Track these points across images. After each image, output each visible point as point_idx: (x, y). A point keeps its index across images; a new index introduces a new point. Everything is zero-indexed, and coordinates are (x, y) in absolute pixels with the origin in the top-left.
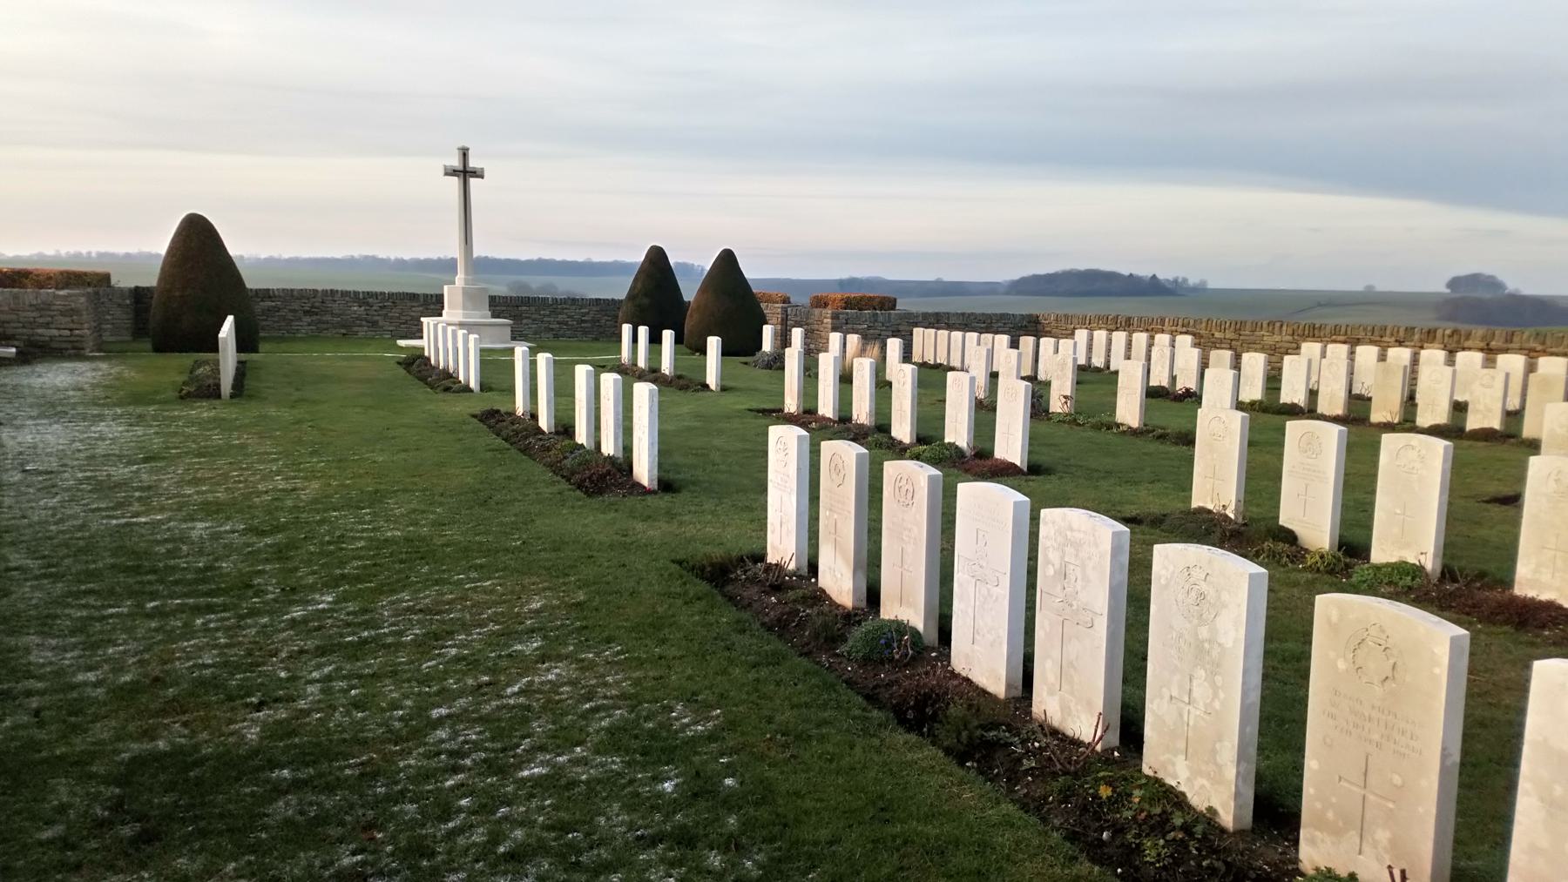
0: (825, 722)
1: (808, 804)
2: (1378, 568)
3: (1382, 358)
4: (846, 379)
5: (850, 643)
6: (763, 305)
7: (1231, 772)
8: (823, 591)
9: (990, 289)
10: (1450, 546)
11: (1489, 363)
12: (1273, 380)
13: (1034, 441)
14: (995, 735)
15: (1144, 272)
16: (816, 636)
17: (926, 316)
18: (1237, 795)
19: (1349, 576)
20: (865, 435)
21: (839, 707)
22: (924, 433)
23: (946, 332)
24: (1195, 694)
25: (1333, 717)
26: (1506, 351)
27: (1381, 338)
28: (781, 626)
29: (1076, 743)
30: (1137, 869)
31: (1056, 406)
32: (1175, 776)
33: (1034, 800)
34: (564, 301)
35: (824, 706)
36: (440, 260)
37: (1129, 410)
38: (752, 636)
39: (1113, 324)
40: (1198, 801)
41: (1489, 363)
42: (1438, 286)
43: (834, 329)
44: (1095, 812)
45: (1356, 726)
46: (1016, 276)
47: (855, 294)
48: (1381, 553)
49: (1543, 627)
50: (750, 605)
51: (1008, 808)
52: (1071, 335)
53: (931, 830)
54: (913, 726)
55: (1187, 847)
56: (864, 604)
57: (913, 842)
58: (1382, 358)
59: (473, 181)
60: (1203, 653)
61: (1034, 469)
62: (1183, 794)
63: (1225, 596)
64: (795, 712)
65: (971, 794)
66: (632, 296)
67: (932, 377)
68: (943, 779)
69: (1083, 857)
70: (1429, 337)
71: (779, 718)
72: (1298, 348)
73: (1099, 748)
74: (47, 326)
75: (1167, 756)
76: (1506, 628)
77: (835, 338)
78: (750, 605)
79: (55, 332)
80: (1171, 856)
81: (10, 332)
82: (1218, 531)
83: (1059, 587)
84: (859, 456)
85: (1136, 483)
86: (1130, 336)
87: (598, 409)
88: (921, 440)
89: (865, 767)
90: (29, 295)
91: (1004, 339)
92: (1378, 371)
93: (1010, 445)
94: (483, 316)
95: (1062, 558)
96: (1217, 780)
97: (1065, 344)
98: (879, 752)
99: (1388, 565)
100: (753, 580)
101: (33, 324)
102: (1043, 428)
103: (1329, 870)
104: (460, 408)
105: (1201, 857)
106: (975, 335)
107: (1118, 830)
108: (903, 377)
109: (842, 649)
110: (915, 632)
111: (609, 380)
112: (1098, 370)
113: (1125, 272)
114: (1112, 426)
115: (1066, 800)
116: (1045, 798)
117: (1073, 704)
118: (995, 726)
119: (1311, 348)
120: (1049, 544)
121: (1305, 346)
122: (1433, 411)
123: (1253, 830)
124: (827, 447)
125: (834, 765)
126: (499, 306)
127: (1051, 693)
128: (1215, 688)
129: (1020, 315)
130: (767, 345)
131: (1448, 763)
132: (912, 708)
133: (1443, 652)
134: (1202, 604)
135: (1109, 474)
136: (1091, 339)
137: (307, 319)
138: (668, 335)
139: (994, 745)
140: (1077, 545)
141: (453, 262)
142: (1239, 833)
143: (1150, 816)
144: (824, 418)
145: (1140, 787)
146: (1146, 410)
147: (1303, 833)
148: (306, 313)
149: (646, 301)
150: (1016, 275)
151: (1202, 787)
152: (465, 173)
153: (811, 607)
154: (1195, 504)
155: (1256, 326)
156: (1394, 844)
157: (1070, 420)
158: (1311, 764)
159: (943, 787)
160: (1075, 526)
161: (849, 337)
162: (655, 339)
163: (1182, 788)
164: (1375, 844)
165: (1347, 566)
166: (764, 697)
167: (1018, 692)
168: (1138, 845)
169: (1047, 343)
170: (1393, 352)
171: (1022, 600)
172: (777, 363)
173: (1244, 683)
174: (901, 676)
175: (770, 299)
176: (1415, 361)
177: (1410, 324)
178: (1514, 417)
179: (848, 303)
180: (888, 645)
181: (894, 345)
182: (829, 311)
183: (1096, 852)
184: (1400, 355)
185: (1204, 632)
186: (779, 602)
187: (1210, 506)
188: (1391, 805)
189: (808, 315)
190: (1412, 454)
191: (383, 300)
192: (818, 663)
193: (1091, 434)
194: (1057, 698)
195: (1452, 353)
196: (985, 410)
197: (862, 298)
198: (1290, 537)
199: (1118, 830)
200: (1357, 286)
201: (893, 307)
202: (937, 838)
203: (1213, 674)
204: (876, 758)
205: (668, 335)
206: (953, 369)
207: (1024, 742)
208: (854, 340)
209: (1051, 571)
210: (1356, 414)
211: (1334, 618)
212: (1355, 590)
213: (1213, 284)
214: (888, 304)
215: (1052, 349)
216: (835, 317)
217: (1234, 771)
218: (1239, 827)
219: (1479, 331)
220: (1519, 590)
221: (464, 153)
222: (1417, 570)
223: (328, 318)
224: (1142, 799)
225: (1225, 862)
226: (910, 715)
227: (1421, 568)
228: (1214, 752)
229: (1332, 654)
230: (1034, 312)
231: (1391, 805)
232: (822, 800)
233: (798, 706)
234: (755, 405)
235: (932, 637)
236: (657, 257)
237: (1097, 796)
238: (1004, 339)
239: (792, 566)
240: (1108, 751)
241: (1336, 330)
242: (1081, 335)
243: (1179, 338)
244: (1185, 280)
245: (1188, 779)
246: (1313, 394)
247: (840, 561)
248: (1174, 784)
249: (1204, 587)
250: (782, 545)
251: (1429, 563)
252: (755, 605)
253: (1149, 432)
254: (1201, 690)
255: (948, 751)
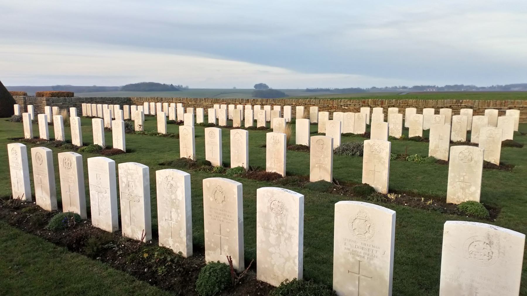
0: (37, 257)
1: (27, 289)
2: (233, 169)
3: (236, 108)
4: (51, 125)
5: (49, 224)
6: (14, 97)
7: (185, 239)
8: (39, 206)
9: (115, 89)
10: (251, 161)
11: (262, 108)
12: (206, 116)
13: (127, 141)
14: (108, 247)
15: (168, 83)
16: (35, 224)
17: (86, 99)
18: (187, 246)
19: (225, 173)
20: (61, 145)
21: (43, 249)
22: (85, 142)
23: (95, 105)
24: (172, 217)
25: (211, 215)
26: (267, 105)
27: (235, 102)
28: (19, 224)
29: (137, 241)
30: (156, 278)
31: (137, 128)
32: (169, 245)
33: (121, 265)
35: (37, 250)
37: (162, 128)
38: (4, 229)
39: (157, 100)
40: (176, 251)
41: (262, 108)
42: (252, 87)
43: (48, 105)
44: (143, 263)
45: (217, 217)
46: (124, 84)
47: (57, 91)
48: (233, 165)
49: (273, 180)
50: (4, 217)
51: (111, 270)
52: (142, 104)
53: (80, 286)
54: (76, 250)
55: (172, 267)
56: (56, 209)
57: (72, 292)
58: (236, 108)
60: (173, 203)
61: (128, 151)
62: (172, 250)
63: (178, 184)
64: (23, 256)
65: (98, 269)
67: (86, 123)
68: (86, 266)
69: (136, 280)
70: (247, 101)
71: (16, 259)
72: (484, 112)
73: (144, 241)
75: (166, 239)
76: (265, 181)
77: (47, 109)
78: (4, 217)
80: (167, 271)
82: (188, 164)
83: (127, 190)
84: (48, 152)
85: (164, 152)
86: (162, 104)
88: (84, 144)
89: (53, 269)
91: (117, 107)
92: (235, 112)
93: (119, 143)
95: (127, 180)
96: (181, 243)
97: (140, 108)
98: (59, 262)
99: (235, 168)
100: (6, 207)
102: (132, 136)
103: (212, 262)
105: (176, 268)
106: (107, 105)
107: (150, 267)
108: (75, 121)
109: (47, 227)
110: (77, 215)
112: (153, 116)
113: (162, 83)
114: (157, 134)
115: (133, 262)
116: (125, 263)
117: (135, 229)
118: (108, 242)
119: (216, 106)
120: (122, 175)
121: (362, 109)
122: (249, 124)
123: (193, 256)
125: (39, 272)
127: (128, 227)
128: (178, 214)
129: (124, 98)
130: (17, 112)
131: (240, 222)
132: (75, 243)
133: (236, 190)
134: (172, 188)
135: (155, 150)
136: (156, 106)
139: (106, 250)
140: (132, 175)
142: (189, 257)
143: (160, 260)
144: (43, 139)
145: (157, 251)
146: (167, 128)
147: (206, 253)
150: (124, 84)
151: (177, 246)
153: (32, 213)
154: (181, 157)
155: (201, 100)
156: (229, 249)
157: (142, 133)
158: (206, 231)
159: (86, 269)
160: (130, 168)
163: (171, 248)
164: (224, 250)
165: (225, 170)
166: (10, 252)
167: (117, 229)
168: (156, 270)
169: (133, 107)
170: (238, 106)
171: (116, 197)
172: (20, 120)
173: (186, 211)
174: (73, 234)
175: (17, 94)
176: (244, 109)
178: (268, 123)
179: (53, 95)
180: (66, 222)
181: (73, 110)
182: (44, 98)
183: (142, 276)
184: (240, 107)
185: (173, 197)
186: (18, 213)
187: (185, 157)
188: (227, 238)
189: (35, 100)
190: (238, 135)
192: (36, 235)
193: (150, 137)
194: (130, 228)
195: (253, 106)
196: (108, 132)
197: (59, 93)
198: (209, 163)
199: (150, 267)
200: (231, 87)
202: (82, 288)
203: (177, 209)
204: (58, 265)
206: (94, 117)
207: (118, 246)
208: (55, 109)
209: (124, 185)
210: (230, 125)
211: (208, 186)
212: (226, 177)
213: (190, 87)
214: (70, 95)
215: (135, 109)
216: (47, 100)
217: (186, 239)
218: (189, 256)
219: (260, 99)
220: (267, 171)
222: (242, 169)
224: (158, 255)
225: (184, 268)
226: (74, 246)
227: (243, 168)
228: (180, 234)
229: (209, 197)
230: (129, 97)
231: (227, 238)
232: (33, 286)
233: (25, 253)
234: (10, 137)
235: (85, 216)
237: (143, 259)
238: (117, 107)
239: (24, 199)
240: (148, 242)
241: (223, 101)
242: (146, 104)
243: (178, 104)
244: (182, 86)
245: (173, 245)
246: (217, 120)
247: (44, 194)
248: (168, 247)
249: (172, 182)
250: (19, 190)
251: (245, 166)
252: (7, 217)
253: (169, 135)
254: (174, 215)
255: (89, 256)
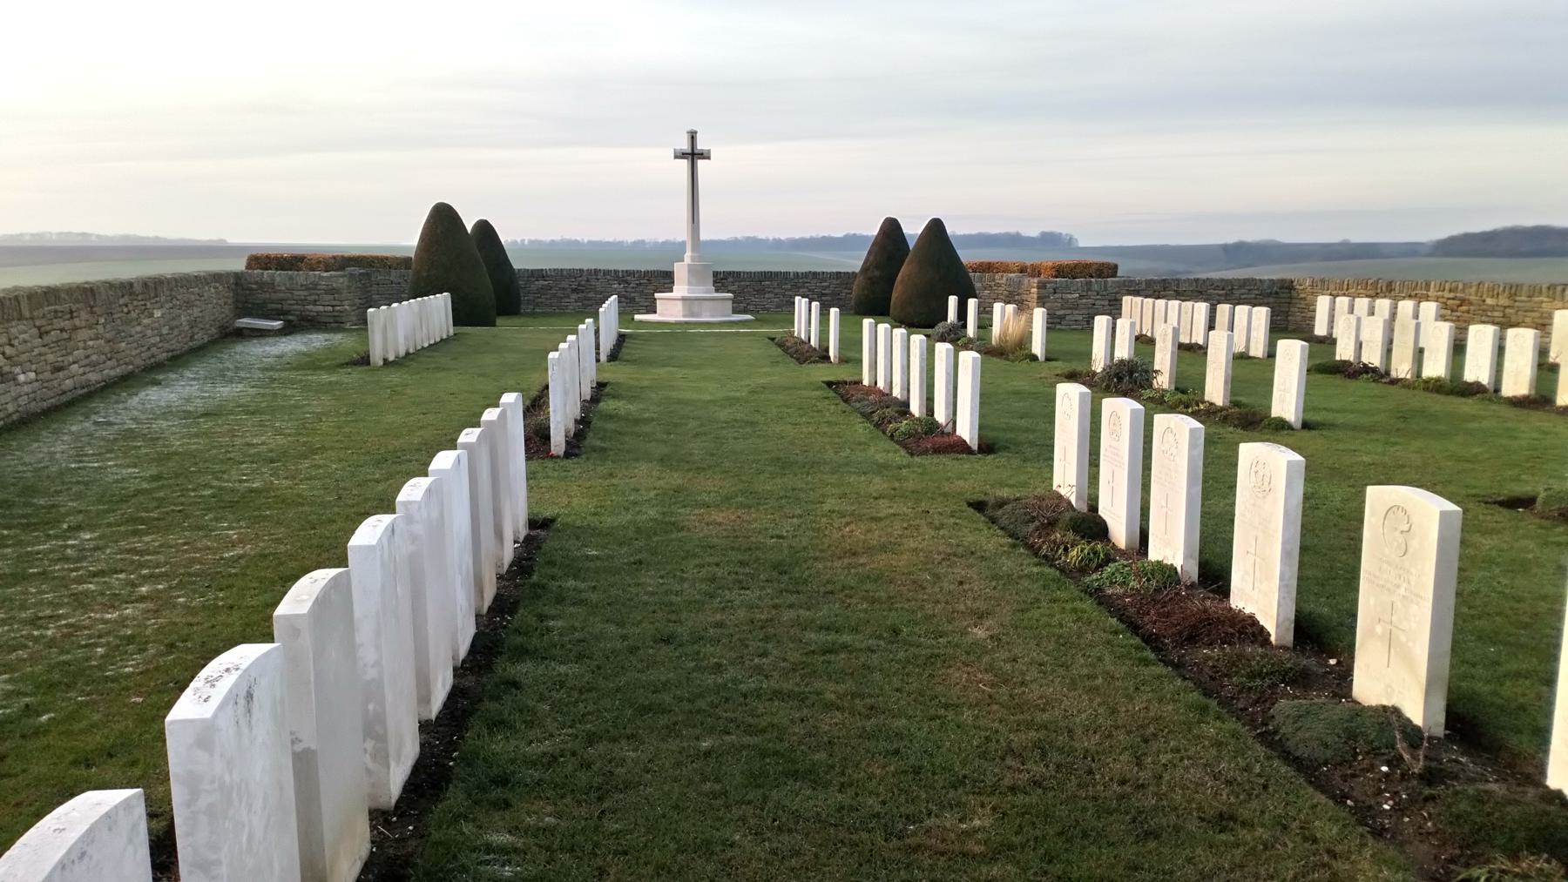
34: (806, 275)
36: (812, 239)
59: (700, 163)
66: (865, 269)
74: (315, 303)
79: (321, 308)
81: (286, 307)
87: (932, 378)
90: (301, 277)
94: (706, 290)
101: (304, 302)
104: (821, 373)
111: (943, 349)
124: (1161, 420)
126: (722, 280)
130: (952, 315)
137: (574, 296)
138: (834, 311)
141: (683, 244)
148: (574, 291)
149: (877, 273)
152: (694, 155)
161: (1238, 308)
162: (824, 314)
177: (1553, 281)
179: (1060, 271)
191: (640, 278)
201: (1114, 274)
205: (834, 311)
216: (1041, 286)
221: (693, 137)
223: (591, 295)
236: (892, 228)
